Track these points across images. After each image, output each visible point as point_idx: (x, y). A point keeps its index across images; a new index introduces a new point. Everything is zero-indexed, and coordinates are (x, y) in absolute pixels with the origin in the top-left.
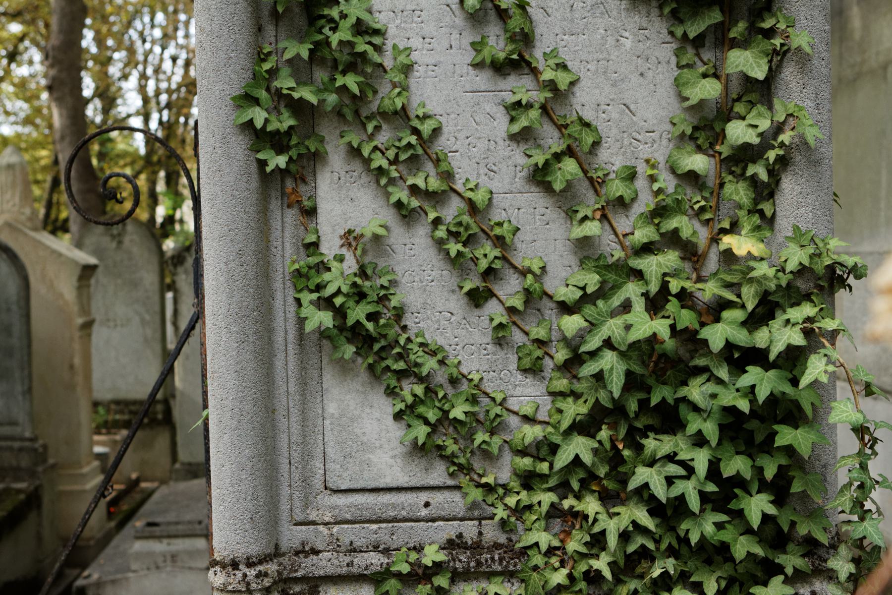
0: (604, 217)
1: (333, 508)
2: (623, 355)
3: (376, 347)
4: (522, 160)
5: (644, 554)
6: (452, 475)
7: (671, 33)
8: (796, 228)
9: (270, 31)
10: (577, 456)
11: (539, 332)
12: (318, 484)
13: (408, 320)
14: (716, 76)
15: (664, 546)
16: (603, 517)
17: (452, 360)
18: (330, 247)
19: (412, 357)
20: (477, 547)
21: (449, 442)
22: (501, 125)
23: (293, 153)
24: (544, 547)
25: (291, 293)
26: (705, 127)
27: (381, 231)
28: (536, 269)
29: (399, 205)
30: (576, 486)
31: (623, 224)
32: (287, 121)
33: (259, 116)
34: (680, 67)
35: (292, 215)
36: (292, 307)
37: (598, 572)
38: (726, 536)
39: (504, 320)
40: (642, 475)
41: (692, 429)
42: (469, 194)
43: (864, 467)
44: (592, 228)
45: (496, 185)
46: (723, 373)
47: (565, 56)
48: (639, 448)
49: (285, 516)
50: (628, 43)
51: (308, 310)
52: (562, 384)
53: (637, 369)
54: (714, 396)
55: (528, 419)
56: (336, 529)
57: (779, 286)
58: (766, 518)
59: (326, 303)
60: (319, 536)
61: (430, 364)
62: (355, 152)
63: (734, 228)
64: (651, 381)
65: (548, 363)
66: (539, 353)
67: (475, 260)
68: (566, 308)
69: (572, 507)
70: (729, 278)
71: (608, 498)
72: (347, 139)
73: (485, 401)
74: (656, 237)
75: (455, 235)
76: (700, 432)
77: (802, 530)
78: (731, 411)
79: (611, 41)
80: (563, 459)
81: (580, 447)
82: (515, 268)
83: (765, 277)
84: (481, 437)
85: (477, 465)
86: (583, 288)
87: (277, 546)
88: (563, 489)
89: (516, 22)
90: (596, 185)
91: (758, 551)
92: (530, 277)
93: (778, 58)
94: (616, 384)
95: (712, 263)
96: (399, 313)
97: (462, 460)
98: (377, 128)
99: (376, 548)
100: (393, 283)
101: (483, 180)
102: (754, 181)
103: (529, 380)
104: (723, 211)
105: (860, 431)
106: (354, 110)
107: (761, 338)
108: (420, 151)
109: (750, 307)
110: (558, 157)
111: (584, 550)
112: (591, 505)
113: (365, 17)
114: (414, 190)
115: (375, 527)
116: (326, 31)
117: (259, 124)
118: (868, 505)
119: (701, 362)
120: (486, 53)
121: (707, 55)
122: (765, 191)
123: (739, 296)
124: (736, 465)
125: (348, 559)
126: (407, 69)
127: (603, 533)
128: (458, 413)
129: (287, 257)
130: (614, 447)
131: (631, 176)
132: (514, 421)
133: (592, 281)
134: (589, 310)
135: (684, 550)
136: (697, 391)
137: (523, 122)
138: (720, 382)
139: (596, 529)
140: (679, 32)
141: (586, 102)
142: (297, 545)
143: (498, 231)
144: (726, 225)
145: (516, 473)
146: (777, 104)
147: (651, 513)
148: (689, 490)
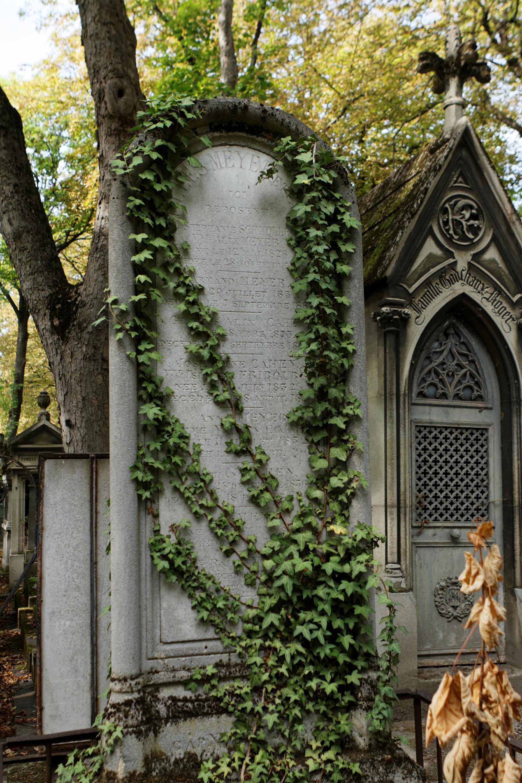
0: (281, 517)
1: (165, 651)
2: (291, 577)
3: (185, 576)
4: (246, 493)
5: (301, 665)
6: (217, 633)
7: (307, 440)
8: (359, 522)
9: (142, 436)
10: (272, 623)
11: (254, 568)
12: (157, 640)
13: (198, 564)
14: (324, 458)
15: (308, 660)
16: (283, 649)
17: (217, 581)
18: (165, 531)
19: (201, 580)
20: (228, 666)
21: (216, 618)
22: (238, 477)
23: (152, 490)
24: (259, 664)
25: (149, 553)
26: (321, 479)
27: (188, 524)
28: (253, 540)
29: (196, 513)
30: (271, 635)
31: (288, 520)
32: (149, 477)
33: (140, 475)
34: (310, 453)
35: (150, 517)
36: (149, 560)
37: (282, 674)
38: (335, 654)
39: (240, 563)
40: (299, 629)
41: (320, 608)
42: (225, 508)
43: (391, 621)
44: (277, 522)
45: (235, 504)
46: (332, 584)
47: (264, 448)
48: (297, 618)
49: (144, 656)
50: (289, 443)
51: (157, 561)
52: (264, 590)
53: (297, 583)
54: (328, 594)
55: (250, 607)
56: (166, 661)
57: (353, 546)
58: (351, 645)
59: (164, 557)
60: (158, 664)
61: (209, 584)
62: (176, 489)
63: (333, 521)
64: (302, 588)
65: (258, 581)
66: (254, 577)
67: (227, 537)
68: (265, 557)
69: (269, 645)
70: (332, 543)
71: (285, 641)
72: (173, 484)
73: (231, 599)
74: (302, 526)
75: (219, 526)
76: (323, 610)
77: (365, 650)
78: (336, 600)
79: (282, 442)
80: (266, 624)
81: (273, 618)
82: (243, 539)
83: (347, 543)
84: (230, 616)
85: (228, 628)
86: (273, 548)
87: (140, 671)
88: (265, 637)
89: (245, 436)
90: (276, 503)
91: (348, 660)
92: (251, 544)
93: (351, 452)
94: (289, 590)
95: (324, 537)
96: (194, 561)
97: (222, 626)
98: (186, 479)
99: (184, 669)
100: (192, 547)
101: (230, 501)
102: (341, 503)
103: (250, 589)
104: (328, 514)
105: (390, 607)
106: (176, 472)
107: (346, 568)
108: (205, 489)
109: (342, 555)
110: (262, 492)
111: (275, 664)
112: (277, 644)
113: (182, 431)
114: (202, 506)
115: (183, 659)
116: (166, 436)
117: (140, 479)
118: (393, 637)
119: (322, 579)
120: (232, 447)
121: (321, 449)
122: (345, 506)
123: (336, 550)
124: (338, 623)
125: (172, 674)
126: (199, 453)
127: (284, 656)
128: (220, 604)
129: (148, 537)
130: (287, 617)
131: (291, 499)
132: (243, 608)
133: (277, 545)
134: (276, 558)
135: (316, 662)
136: (321, 591)
137: (247, 477)
138: (330, 587)
139: (281, 654)
140: (310, 439)
141: (273, 467)
142: (148, 669)
143: (237, 524)
144: (329, 520)
145: (244, 631)
146: (350, 470)
147: (303, 646)
148: (319, 634)
